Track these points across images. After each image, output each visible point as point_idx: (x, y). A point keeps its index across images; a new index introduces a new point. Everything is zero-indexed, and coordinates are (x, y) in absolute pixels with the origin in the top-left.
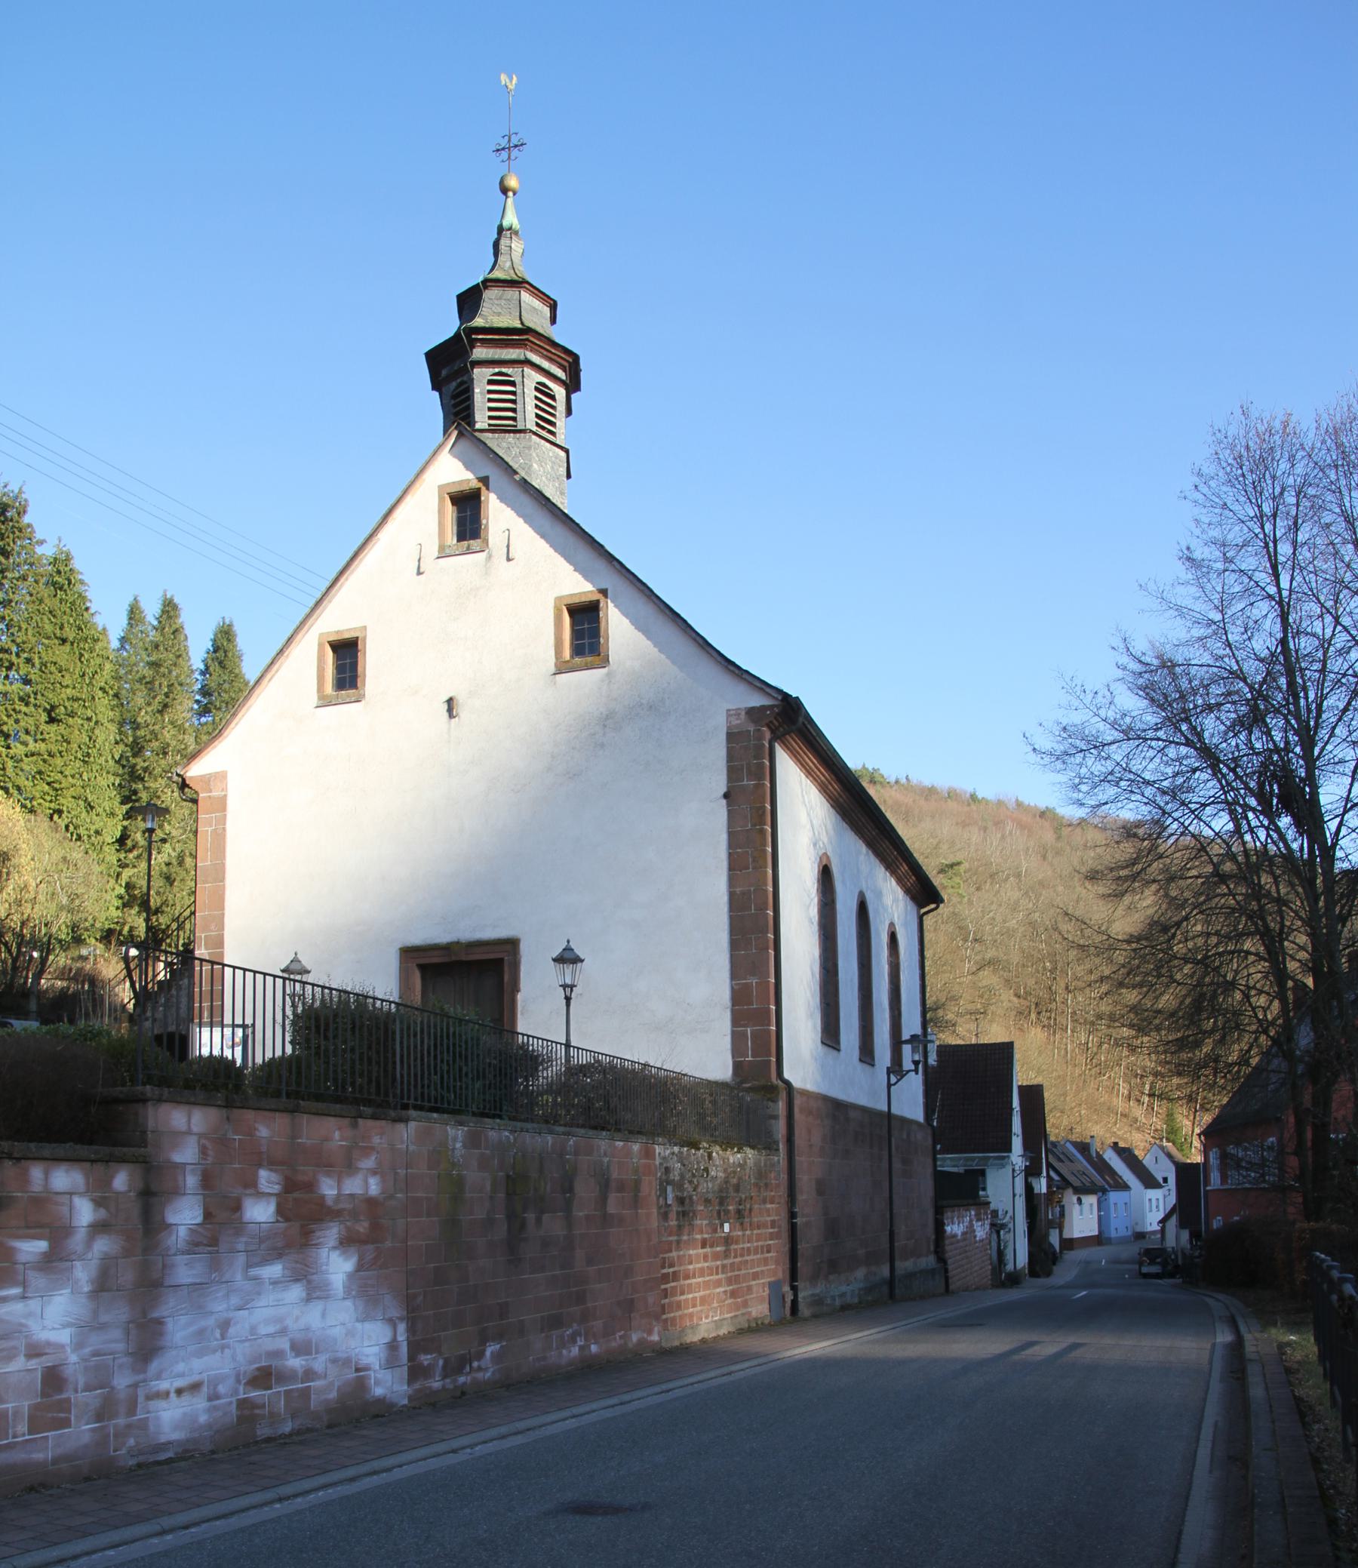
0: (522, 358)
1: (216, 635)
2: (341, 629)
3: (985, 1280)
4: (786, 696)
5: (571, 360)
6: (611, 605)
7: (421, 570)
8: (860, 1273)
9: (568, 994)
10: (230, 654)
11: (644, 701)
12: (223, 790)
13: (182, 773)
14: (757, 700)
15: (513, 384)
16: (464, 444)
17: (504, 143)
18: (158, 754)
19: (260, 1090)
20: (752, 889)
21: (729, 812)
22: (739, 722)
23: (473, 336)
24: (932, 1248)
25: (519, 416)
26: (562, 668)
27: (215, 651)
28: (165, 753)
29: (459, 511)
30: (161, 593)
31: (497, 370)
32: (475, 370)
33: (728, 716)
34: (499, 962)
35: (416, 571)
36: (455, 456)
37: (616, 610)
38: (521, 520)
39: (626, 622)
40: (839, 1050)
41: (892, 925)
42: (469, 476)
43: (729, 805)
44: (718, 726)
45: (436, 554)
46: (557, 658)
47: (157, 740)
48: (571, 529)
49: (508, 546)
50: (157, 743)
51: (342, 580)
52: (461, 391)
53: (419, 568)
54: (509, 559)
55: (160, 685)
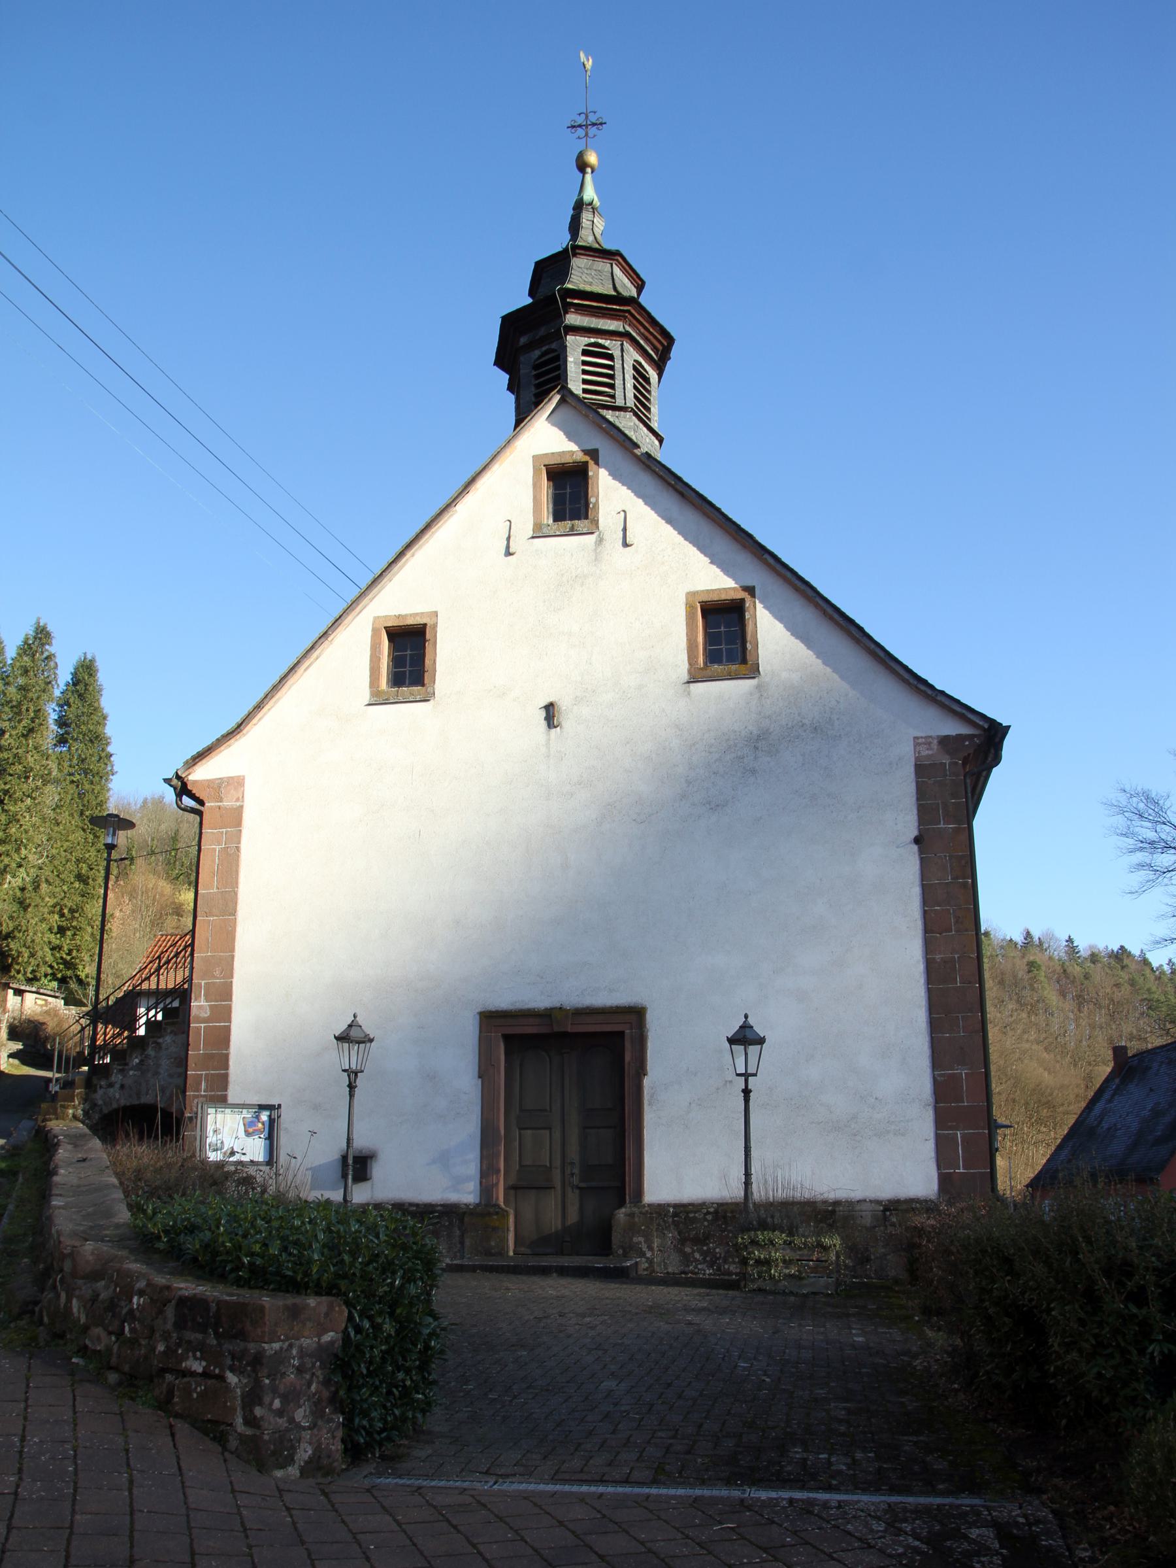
0: (621, 329)
1: (76, 669)
2: (403, 613)
5: (666, 344)
6: (759, 606)
7: (511, 550)
10: (91, 688)
11: (805, 721)
12: (238, 800)
13: (183, 776)
14: (952, 728)
15: (610, 357)
16: (565, 411)
17: (581, 120)
18: (19, 778)
20: (956, 956)
21: (922, 860)
22: (930, 752)
23: (568, 300)
25: (619, 393)
26: (695, 677)
27: (75, 685)
28: (27, 778)
29: (556, 488)
30: (34, 621)
31: (592, 340)
32: (568, 337)
33: (916, 745)
35: (503, 551)
36: (554, 424)
37: (767, 612)
38: (640, 502)
39: (779, 627)
42: (573, 447)
43: (921, 852)
44: (905, 753)
45: (531, 534)
46: (690, 664)
47: (20, 764)
48: (705, 515)
49: (625, 530)
50: (20, 767)
51: (409, 555)
52: (541, 363)
53: (508, 547)
54: (625, 544)
55: (27, 710)
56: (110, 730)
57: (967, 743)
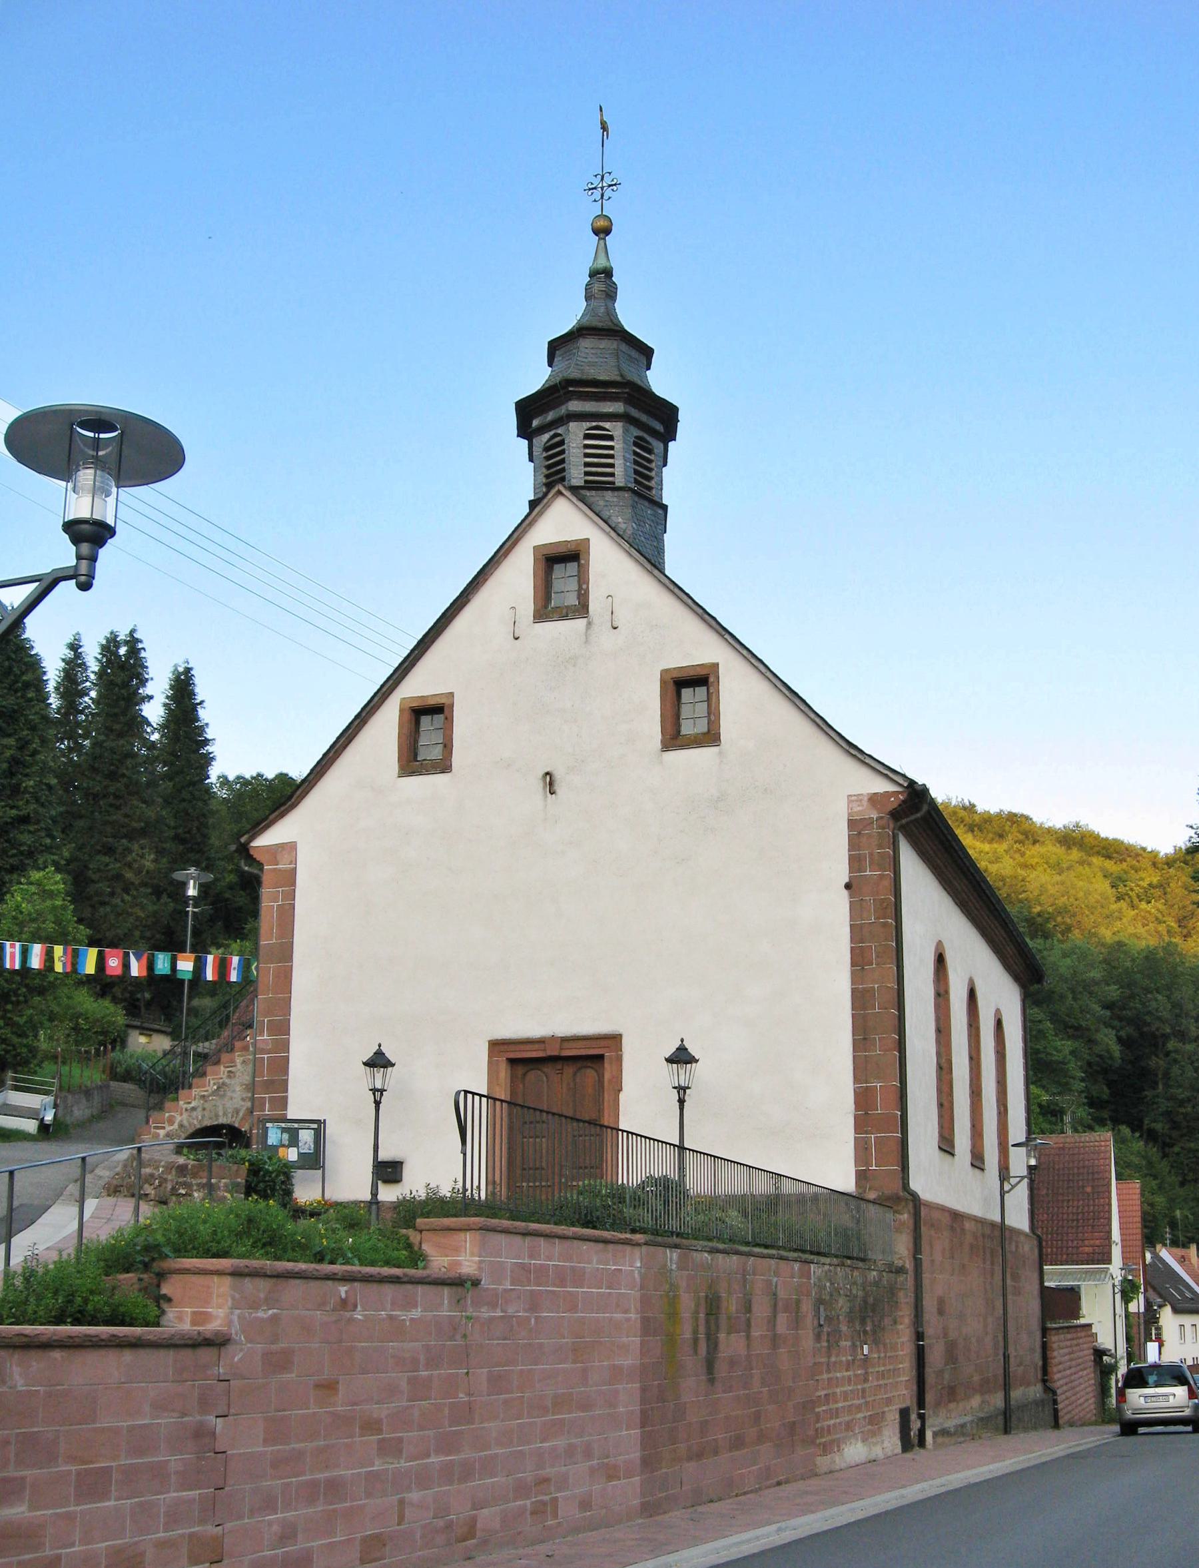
3: (1089, 1416)
4: (912, 783)
8: (976, 1401)
9: (681, 1096)
14: (882, 786)
19: (282, 1178)
20: (876, 986)
24: (1040, 1376)
31: (594, 424)
33: (850, 802)
34: (600, 1058)
40: (953, 1155)
41: (998, 1011)
43: (851, 896)
56: (3, 1276)
57: (893, 799)
